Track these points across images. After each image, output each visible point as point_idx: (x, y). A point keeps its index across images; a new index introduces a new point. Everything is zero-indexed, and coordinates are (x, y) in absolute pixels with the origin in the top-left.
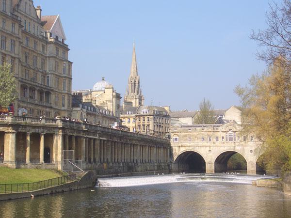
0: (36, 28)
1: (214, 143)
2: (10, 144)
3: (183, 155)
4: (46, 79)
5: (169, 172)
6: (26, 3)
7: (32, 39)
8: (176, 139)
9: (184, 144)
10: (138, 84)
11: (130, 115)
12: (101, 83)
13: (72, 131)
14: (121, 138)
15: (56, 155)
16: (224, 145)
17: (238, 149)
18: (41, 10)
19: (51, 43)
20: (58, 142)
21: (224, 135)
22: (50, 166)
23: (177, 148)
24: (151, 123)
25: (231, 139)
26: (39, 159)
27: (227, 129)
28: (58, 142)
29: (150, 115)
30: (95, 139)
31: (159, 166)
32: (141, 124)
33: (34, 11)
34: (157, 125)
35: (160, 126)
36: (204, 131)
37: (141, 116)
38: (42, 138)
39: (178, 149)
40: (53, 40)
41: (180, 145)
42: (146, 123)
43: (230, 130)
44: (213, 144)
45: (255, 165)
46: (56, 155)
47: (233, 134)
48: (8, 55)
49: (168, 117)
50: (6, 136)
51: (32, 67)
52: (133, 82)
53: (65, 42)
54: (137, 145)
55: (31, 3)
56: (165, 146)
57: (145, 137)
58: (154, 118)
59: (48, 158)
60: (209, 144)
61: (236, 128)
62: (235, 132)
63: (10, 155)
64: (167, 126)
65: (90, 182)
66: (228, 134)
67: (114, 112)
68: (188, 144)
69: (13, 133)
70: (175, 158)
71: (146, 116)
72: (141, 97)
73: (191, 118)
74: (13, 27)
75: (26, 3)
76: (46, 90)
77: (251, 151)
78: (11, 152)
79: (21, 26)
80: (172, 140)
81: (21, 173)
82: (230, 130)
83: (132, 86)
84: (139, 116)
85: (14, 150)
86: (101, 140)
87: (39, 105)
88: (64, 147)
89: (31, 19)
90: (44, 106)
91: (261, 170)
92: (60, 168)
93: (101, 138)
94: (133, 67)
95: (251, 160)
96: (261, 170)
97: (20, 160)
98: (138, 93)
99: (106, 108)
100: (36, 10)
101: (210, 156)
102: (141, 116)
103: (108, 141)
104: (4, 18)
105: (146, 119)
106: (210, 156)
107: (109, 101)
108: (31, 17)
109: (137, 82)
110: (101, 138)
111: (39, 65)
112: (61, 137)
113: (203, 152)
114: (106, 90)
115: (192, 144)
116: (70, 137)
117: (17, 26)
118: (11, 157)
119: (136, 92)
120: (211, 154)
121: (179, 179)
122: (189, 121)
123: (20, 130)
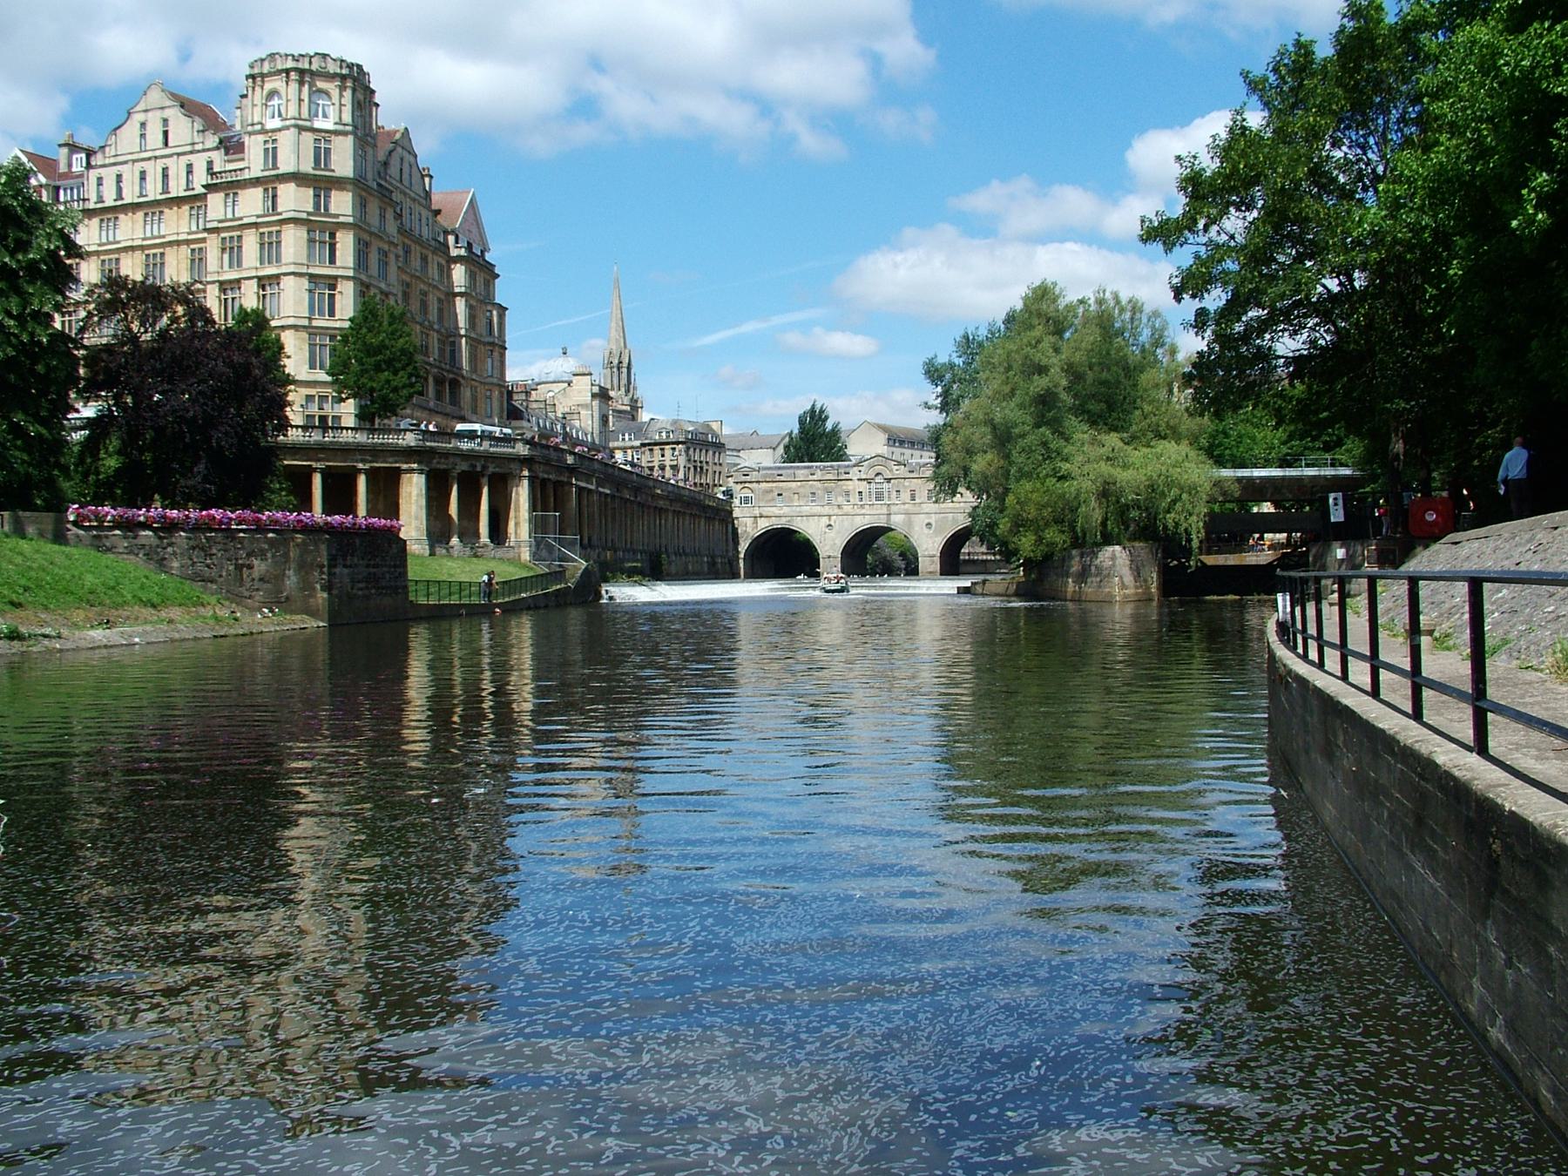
0: (424, 221)
1: (839, 506)
2: (414, 498)
3: (762, 540)
4: (448, 349)
5: (732, 575)
6: (402, 159)
7: (418, 248)
8: (747, 500)
9: (766, 511)
10: (629, 368)
11: (628, 444)
12: (561, 360)
13: (548, 468)
14: (637, 490)
15: (517, 524)
16: (863, 511)
17: (897, 520)
18: (431, 177)
19: (459, 259)
20: (521, 495)
21: (863, 486)
22: (500, 552)
23: (749, 521)
24: (682, 461)
25: (879, 497)
26: (478, 536)
27: (871, 474)
28: (521, 495)
29: (678, 443)
30: (590, 491)
31: (713, 564)
32: (656, 464)
33: (420, 180)
34: (695, 467)
35: (701, 468)
36: (815, 477)
37: (656, 444)
38: (362, 482)
39: (751, 523)
40: (463, 252)
41: (757, 512)
42: (668, 463)
43: (878, 474)
44: (836, 511)
45: (937, 560)
46: (517, 524)
47: (886, 485)
48: (375, 287)
49: (719, 447)
50: (405, 477)
51: (418, 319)
52: (616, 362)
53: (488, 257)
54: (667, 510)
55: (412, 159)
56: (721, 515)
57: (683, 492)
58: (688, 448)
59: (498, 532)
60: (826, 510)
61: (891, 471)
62: (889, 480)
63: (414, 523)
64: (717, 468)
65: (588, 590)
66: (873, 486)
67: (596, 432)
68: (776, 511)
69: (421, 472)
70: (743, 547)
71: (668, 444)
72: (636, 401)
73: (771, 451)
74: (382, 217)
75: (402, 159)
76: (451, 376)
77: (929, 525)
78: (417, 518)
79: (399, 216)
80: (736, 502)
81: (434, 564)
82: (878, 474)
83: (612, 373)
84: (649, 444)
85: (424, 511)
86: (601, 493)
87: (437, 412)
88: (533, 507)
89: (414, 200)
90: (447, 415)
91: (951, 562)
92: (526, 555)
93: (601, 489)
94: (613, 325)
95: (929, 546)
96: (951, 562)
97: (438, 533)
98: (628, 391)
99: (577, 423)
100: (423, 177)
101: (829, 541)
102: (656, 444)
103: (613, 497)
104: (364, 194)
105: (668, 452)
106: (829, 541)
107: (585, 406)
108: (413, 195)
109: (625, 364)
110: (601, 489)
111: (433, 315)
112: (526, 482)
113: (812, 529)
114: (575, 379)
115: (786, 510)
116: (544, 482)
117: (390, 214)
118: (418, 529)
119: (623, 389)
120: (831, 534)
121: (771, 590)
122: (765, 458)
123: (435, 464)
